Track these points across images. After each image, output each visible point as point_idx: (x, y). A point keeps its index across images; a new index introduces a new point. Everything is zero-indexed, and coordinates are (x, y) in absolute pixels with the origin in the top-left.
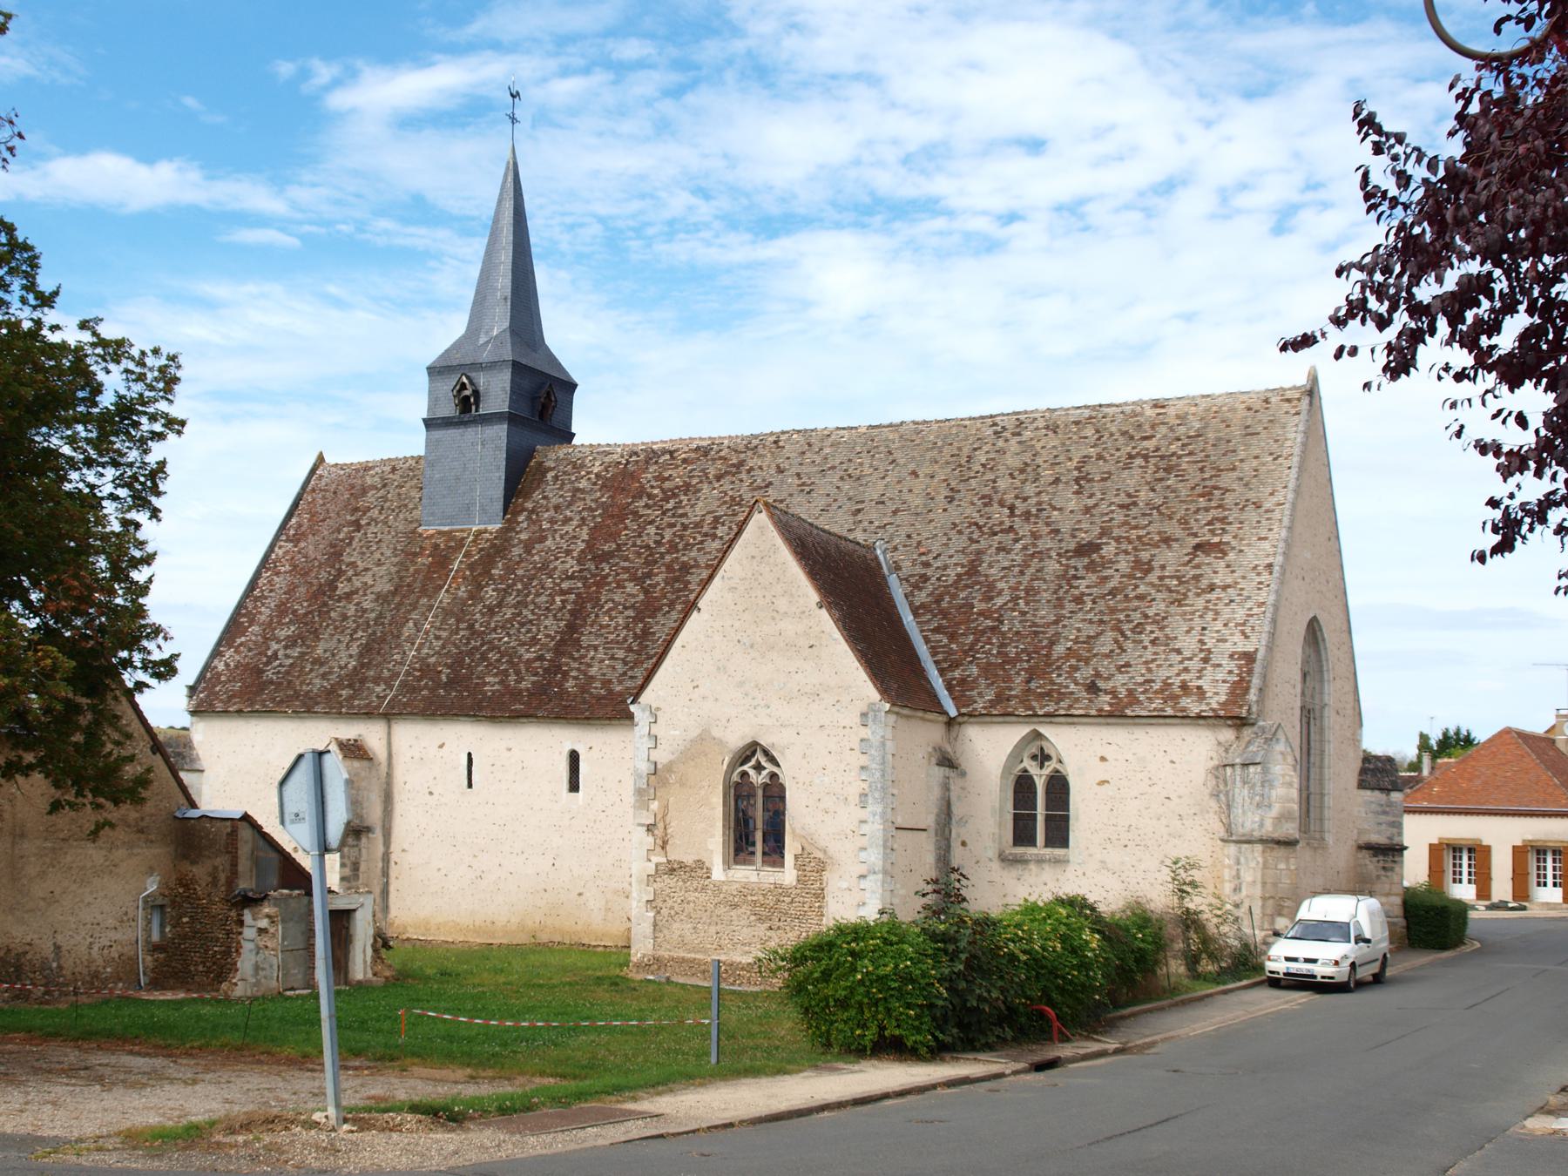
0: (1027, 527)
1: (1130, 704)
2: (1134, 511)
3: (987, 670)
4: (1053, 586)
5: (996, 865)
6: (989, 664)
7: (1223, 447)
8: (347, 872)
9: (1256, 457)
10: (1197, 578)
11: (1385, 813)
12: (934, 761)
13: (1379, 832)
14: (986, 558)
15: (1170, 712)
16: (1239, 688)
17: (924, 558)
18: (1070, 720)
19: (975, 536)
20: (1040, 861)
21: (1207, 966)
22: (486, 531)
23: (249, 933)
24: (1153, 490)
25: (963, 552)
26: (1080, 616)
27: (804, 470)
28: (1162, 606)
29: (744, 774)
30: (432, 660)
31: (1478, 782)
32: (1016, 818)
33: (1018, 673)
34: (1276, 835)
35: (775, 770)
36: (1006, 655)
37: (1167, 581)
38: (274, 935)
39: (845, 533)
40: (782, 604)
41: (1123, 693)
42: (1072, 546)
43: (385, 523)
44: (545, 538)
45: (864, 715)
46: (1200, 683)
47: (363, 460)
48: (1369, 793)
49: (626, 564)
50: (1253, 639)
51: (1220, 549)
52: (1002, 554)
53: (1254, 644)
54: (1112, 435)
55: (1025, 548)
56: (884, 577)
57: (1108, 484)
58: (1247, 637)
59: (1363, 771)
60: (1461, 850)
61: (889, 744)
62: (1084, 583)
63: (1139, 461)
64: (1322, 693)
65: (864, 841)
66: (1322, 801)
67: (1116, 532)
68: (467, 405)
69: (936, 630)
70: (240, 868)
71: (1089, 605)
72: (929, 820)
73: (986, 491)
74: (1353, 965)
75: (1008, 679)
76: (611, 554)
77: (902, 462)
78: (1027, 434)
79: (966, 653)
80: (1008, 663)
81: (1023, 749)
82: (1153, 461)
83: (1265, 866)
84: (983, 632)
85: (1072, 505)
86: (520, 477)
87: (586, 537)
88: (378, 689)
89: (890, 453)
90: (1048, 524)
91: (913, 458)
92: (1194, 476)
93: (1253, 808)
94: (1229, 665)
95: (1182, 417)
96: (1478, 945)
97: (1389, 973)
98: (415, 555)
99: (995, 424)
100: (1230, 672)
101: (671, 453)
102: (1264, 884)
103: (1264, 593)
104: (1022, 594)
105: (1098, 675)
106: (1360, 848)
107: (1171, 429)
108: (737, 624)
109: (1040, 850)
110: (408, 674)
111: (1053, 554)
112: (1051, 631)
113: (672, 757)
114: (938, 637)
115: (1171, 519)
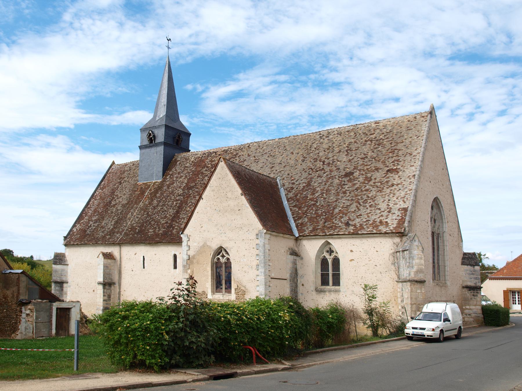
0: (328, 168)
1: (360, 229)
2: (366, 160)
3: (311, 220)
4: (336, 188)
5: (314, 293)
6: (311, 217)
7: (399, 135)
8: (106, 298)
9: (411, 137)
10: (387, 182)
11: (473, 274)
12: (289, 253)
13: (471, 282)
14: (314, 180)
15: (375, 231)
16: (401, 222)
17: (293, 181)
18: (339, 236)
19: (310, 173)
20: (330, 291)
21: (383, 332)
22: (157, 182)
23: (24, 315)
24: (373, 152)
25: (306, 178)
26: (345, 198)
27: (257, 155)
28: (374, 193)
29: (218, 259)
30: (135, 225)
31: (520, 268)
32: (322, 275)
33: (321, 220)
34: (416, 279)
35: (228, 257)
36: (318, 213)
37: (377, 184)
38: (32, 316)
39: (268, 175)
40: (229, 195)
41: (358, 225)
42: (344, 174)
43: (128, 182)
44: (174, 183)
45: (257, 235)
46: (387, 220)
47: (125, 162)
48: (466, 266)
49: (197, 190)
50: (407, 203)
51: (396, 171)
52: (319, 178)
53: (408, 204)
54: (360, 134)
55: (327, 175)
56: (278, 189)
57: (358, 151)
58: (405, 202)
59: (463, 258)
60: (515, 293)
61: (267, 246)
62: (347, 186)
63: (369, 142)
64: (443, 227)
65: (258, 283)
66: (445, 268)
67: (359, 168)
68: (152, 139)
69: (294, 206)
70: (21, 291)
71: (348, 194)
72: (287, 276)
73: (315, 157)
74: (442, 331)
75: (318, 222)
76: (193, 187)
77: (288, 149)
78: (331, 137)
79: (304, 214)
80: (318, 216)
81: (323, 249)
82: (374, 142)
83: (412, 291)
84: (310, 206)
85: (345, 159)
86: (168, 164)
87: (186, 182)
88: (118, 235)
89: (285, 147)
90: (336, 167)
91: (292, 148)
92: (388, 146)
93: (406, 268)
94: (398, 213)
95: (385, 126)
96: (514, 325)
97: (463, 335)
98: (135, 191)
99: (320, 134)
100: (398, 216)
101: (215, 153)
102: (411, 298)
103: (412, 186)
104: (325, 192)
105: (350, 219)
106: (463, 287)
107: (381, 130)
108: (215, 203)
109: (331, 287)
110: (127, 230)
111: (337, 177)
112: (334, 204)
113: (194, 253)
114: (295, 208)
115: (379, 161)
